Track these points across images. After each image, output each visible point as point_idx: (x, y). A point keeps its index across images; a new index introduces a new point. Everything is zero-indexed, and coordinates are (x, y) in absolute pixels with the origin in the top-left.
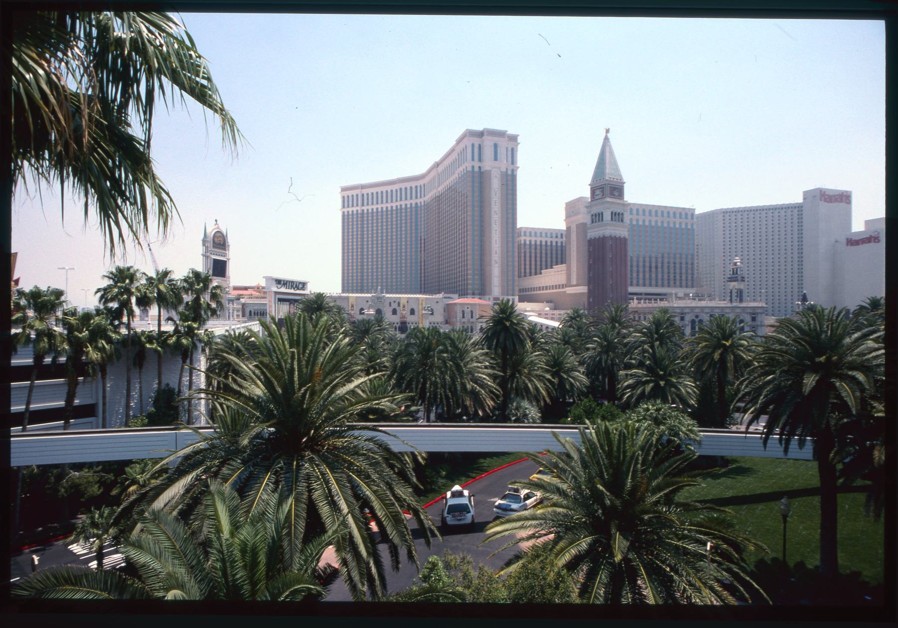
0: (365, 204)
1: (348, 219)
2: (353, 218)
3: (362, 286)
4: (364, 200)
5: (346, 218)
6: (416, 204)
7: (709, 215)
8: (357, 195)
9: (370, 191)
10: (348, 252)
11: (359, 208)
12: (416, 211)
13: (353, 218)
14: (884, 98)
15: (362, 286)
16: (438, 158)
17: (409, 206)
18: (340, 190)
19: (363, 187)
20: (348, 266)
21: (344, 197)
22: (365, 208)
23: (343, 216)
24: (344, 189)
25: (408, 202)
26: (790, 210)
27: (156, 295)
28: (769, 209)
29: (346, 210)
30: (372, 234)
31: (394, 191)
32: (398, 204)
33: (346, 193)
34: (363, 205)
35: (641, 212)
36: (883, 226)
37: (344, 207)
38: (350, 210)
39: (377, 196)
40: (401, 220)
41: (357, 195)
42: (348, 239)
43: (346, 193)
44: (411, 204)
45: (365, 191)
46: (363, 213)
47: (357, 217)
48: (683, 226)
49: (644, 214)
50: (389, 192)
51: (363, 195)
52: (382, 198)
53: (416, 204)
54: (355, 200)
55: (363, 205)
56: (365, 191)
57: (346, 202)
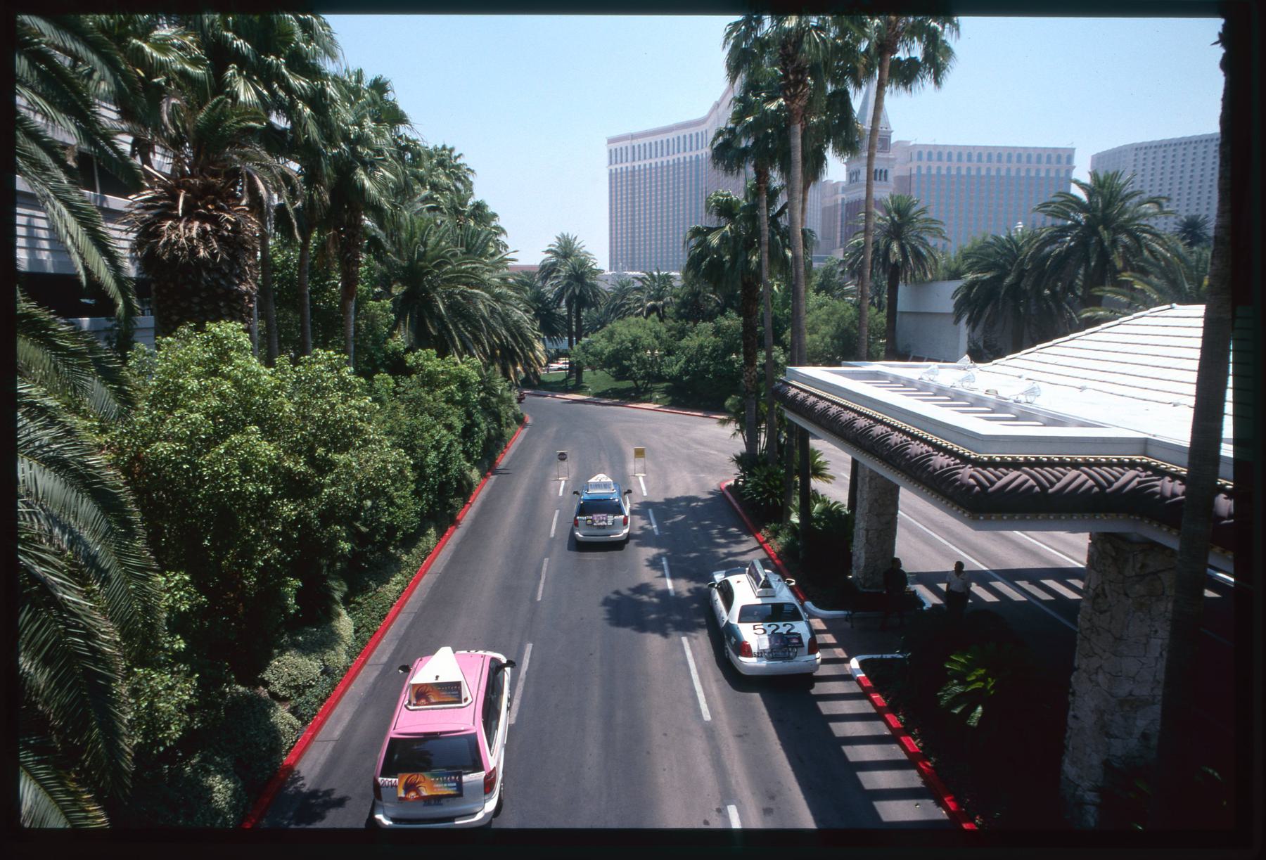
0: (637, 158)
1: (616, 178)
2: (645, 174)
3: (633, 263)
4: (635, 153)
5: (614, 178)
6: (697, 156)
7: (1120, 152)
8: (627, 148)
9: (641, 141)
10: (616, 221)
11: (628, 164)
12: (697, 166)
13: (645, 174)
14: (1177, 19)
15: (633, 263)
16: (718, 99)
17: (688, 159)
18: (606, 142)
19: (633, 137)
20: (617, 238)
21: (611, 151)
22: (636, 164)
23: (611, 174)
24: (611, 141)
25: (647, 162)
26: (1203, 144)
27: (217, 16)
28: (1191, 143)
29: (613, 167)
30: (662, 176)
31: (671, 140)
32: (676, 157)
33: (614, 146)
34: (634, 160)
35: (965, 157)
36: (1210, 168)
37: (611, 163)
38: (618, 166)
39: (679, 143)
40: (679, 177)
41: (627, 148)
42: (616, 208)
43: (614, 146)
44: (691, 157)
45: (636, 142)
46: (633, 171)
47: (627, 176)
48: (973, 173)
49: (969, 160)
50: (688, 136)
51: (634, 147)
52: (656, 150)
53: (697, 156)
54: (659, 148)
55: (634, 160)
56: (636, 142)
57: (614, 157)
